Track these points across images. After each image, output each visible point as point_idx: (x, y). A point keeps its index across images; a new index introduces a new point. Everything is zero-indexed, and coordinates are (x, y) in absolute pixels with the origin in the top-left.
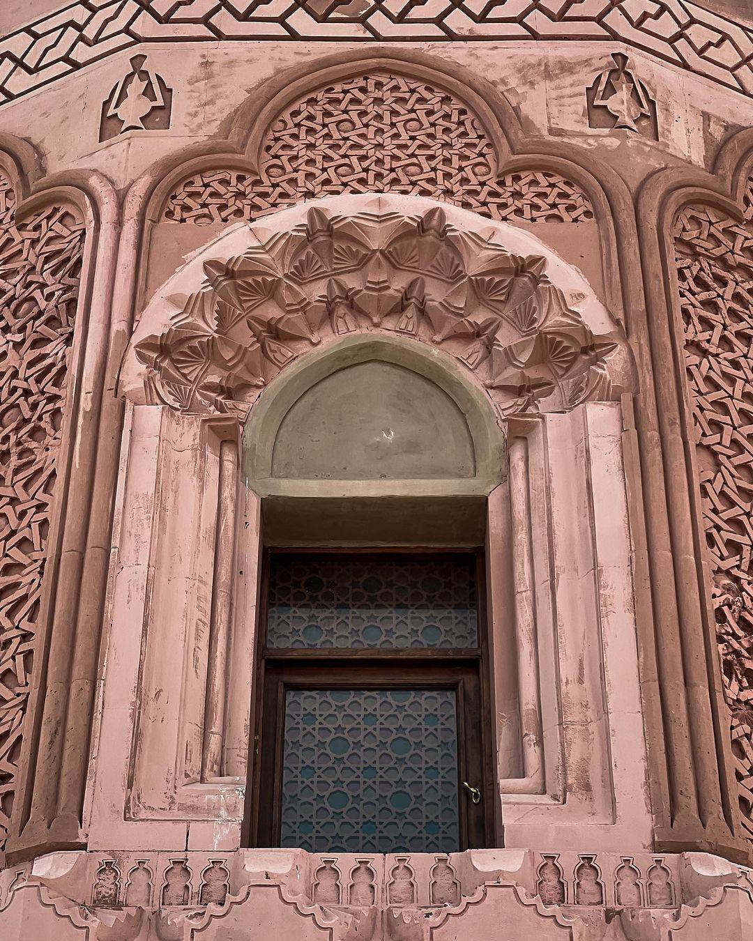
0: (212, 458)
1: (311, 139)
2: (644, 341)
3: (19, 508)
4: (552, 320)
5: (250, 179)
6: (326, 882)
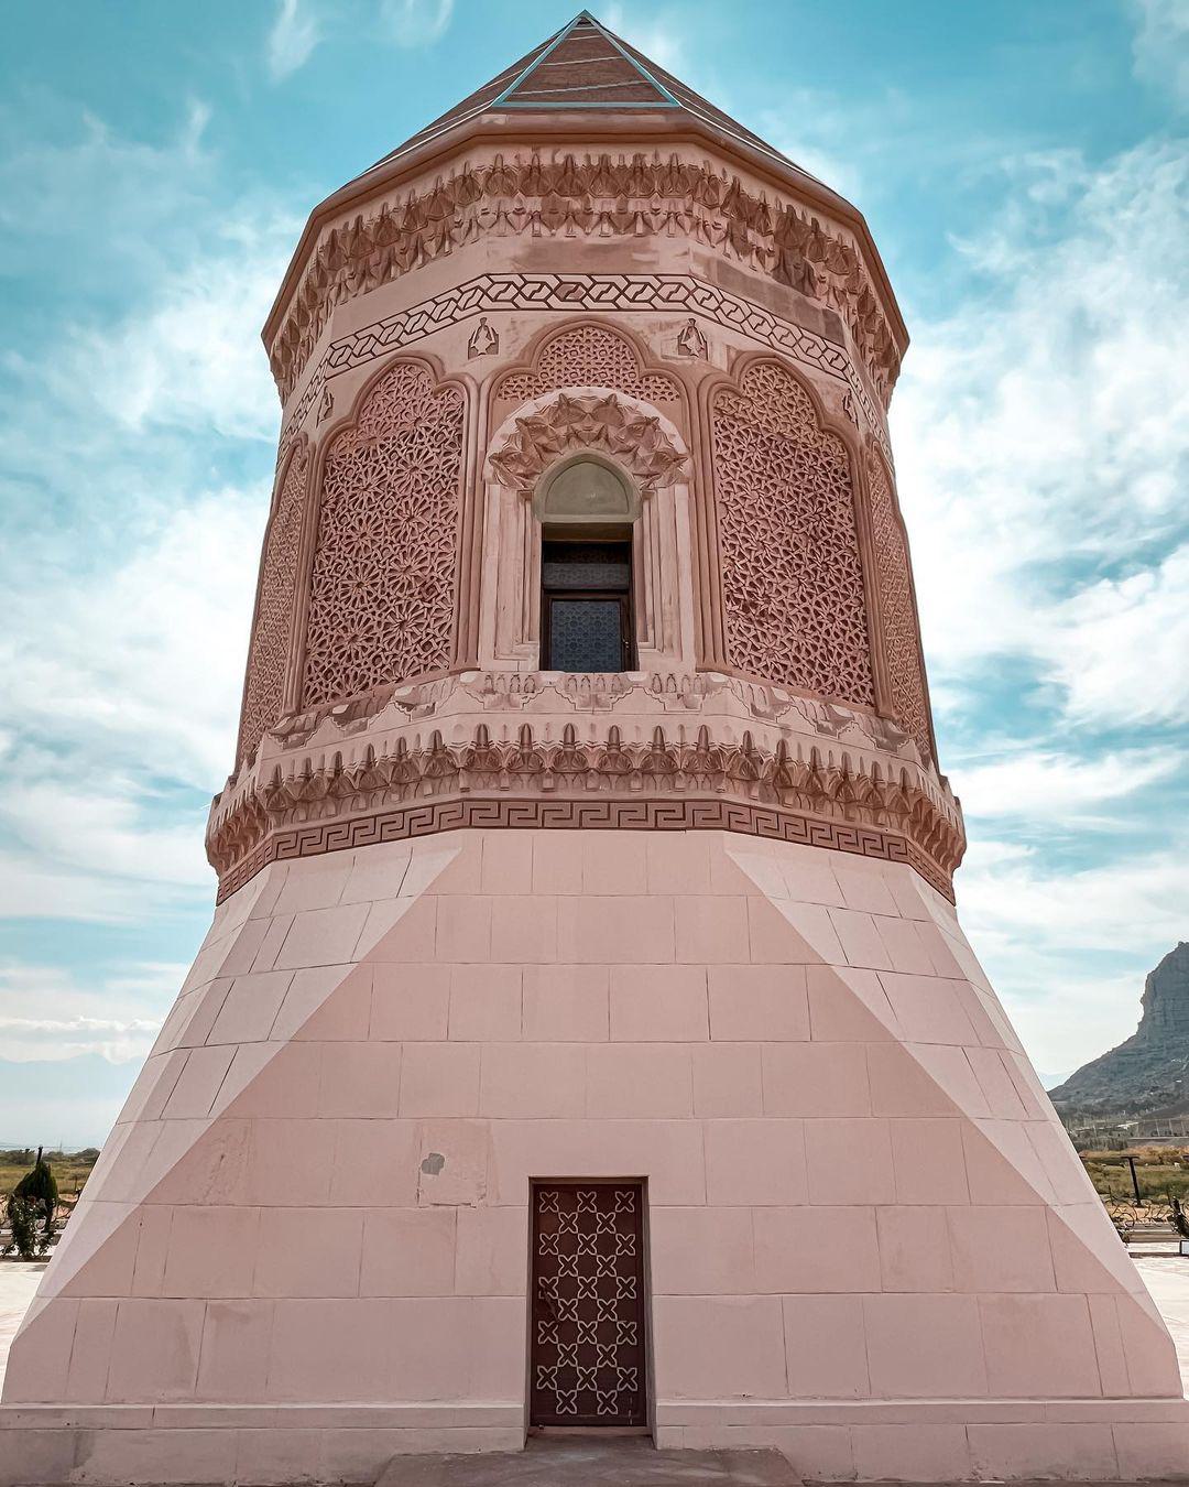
0: (522, 508)
1: (560, 367)
2: (700, 457)
3: (444, 528)
4: (661, 446)
5: (534, 379)
6: (572, 684)
